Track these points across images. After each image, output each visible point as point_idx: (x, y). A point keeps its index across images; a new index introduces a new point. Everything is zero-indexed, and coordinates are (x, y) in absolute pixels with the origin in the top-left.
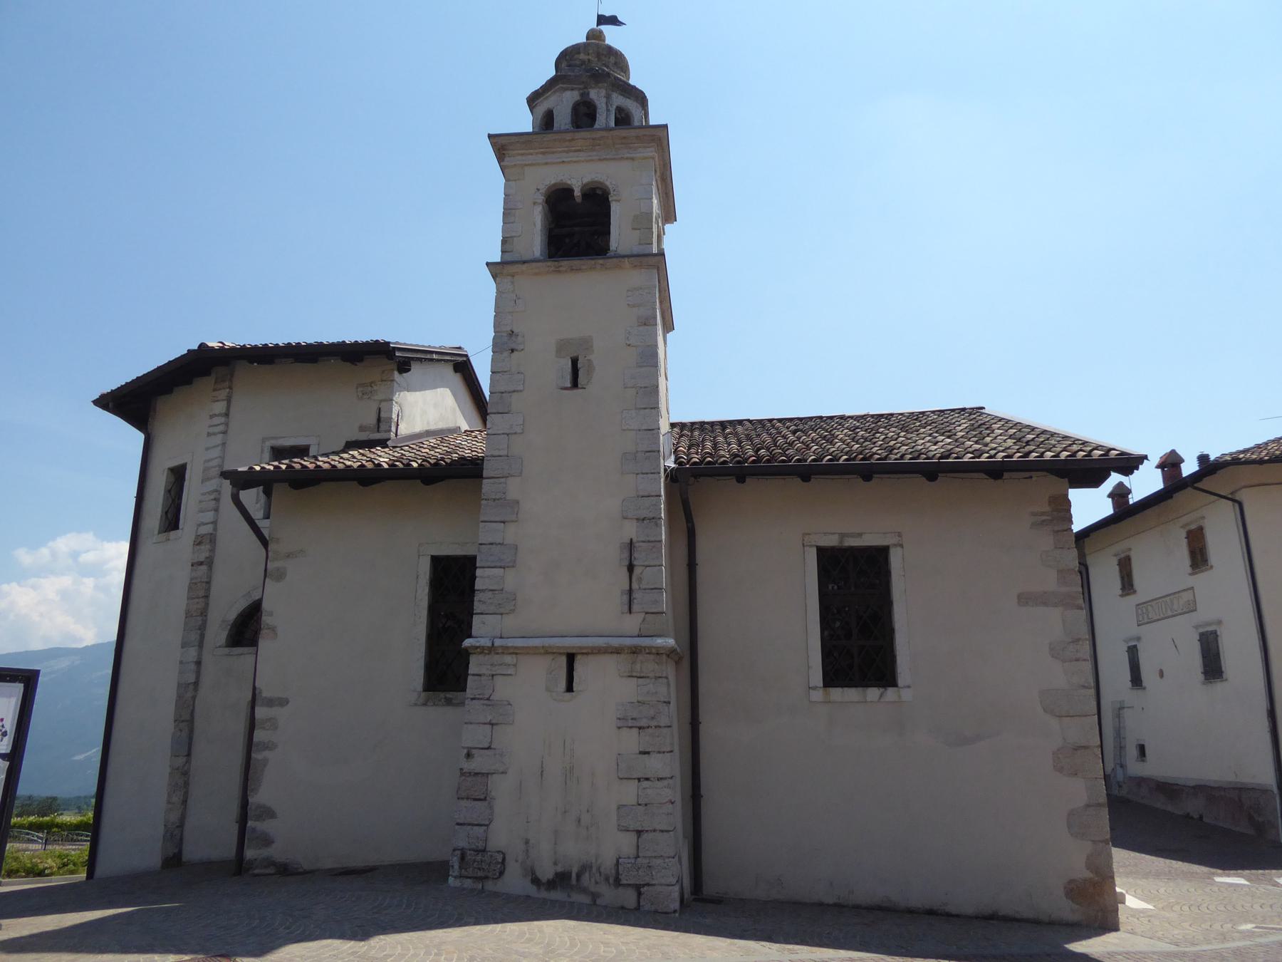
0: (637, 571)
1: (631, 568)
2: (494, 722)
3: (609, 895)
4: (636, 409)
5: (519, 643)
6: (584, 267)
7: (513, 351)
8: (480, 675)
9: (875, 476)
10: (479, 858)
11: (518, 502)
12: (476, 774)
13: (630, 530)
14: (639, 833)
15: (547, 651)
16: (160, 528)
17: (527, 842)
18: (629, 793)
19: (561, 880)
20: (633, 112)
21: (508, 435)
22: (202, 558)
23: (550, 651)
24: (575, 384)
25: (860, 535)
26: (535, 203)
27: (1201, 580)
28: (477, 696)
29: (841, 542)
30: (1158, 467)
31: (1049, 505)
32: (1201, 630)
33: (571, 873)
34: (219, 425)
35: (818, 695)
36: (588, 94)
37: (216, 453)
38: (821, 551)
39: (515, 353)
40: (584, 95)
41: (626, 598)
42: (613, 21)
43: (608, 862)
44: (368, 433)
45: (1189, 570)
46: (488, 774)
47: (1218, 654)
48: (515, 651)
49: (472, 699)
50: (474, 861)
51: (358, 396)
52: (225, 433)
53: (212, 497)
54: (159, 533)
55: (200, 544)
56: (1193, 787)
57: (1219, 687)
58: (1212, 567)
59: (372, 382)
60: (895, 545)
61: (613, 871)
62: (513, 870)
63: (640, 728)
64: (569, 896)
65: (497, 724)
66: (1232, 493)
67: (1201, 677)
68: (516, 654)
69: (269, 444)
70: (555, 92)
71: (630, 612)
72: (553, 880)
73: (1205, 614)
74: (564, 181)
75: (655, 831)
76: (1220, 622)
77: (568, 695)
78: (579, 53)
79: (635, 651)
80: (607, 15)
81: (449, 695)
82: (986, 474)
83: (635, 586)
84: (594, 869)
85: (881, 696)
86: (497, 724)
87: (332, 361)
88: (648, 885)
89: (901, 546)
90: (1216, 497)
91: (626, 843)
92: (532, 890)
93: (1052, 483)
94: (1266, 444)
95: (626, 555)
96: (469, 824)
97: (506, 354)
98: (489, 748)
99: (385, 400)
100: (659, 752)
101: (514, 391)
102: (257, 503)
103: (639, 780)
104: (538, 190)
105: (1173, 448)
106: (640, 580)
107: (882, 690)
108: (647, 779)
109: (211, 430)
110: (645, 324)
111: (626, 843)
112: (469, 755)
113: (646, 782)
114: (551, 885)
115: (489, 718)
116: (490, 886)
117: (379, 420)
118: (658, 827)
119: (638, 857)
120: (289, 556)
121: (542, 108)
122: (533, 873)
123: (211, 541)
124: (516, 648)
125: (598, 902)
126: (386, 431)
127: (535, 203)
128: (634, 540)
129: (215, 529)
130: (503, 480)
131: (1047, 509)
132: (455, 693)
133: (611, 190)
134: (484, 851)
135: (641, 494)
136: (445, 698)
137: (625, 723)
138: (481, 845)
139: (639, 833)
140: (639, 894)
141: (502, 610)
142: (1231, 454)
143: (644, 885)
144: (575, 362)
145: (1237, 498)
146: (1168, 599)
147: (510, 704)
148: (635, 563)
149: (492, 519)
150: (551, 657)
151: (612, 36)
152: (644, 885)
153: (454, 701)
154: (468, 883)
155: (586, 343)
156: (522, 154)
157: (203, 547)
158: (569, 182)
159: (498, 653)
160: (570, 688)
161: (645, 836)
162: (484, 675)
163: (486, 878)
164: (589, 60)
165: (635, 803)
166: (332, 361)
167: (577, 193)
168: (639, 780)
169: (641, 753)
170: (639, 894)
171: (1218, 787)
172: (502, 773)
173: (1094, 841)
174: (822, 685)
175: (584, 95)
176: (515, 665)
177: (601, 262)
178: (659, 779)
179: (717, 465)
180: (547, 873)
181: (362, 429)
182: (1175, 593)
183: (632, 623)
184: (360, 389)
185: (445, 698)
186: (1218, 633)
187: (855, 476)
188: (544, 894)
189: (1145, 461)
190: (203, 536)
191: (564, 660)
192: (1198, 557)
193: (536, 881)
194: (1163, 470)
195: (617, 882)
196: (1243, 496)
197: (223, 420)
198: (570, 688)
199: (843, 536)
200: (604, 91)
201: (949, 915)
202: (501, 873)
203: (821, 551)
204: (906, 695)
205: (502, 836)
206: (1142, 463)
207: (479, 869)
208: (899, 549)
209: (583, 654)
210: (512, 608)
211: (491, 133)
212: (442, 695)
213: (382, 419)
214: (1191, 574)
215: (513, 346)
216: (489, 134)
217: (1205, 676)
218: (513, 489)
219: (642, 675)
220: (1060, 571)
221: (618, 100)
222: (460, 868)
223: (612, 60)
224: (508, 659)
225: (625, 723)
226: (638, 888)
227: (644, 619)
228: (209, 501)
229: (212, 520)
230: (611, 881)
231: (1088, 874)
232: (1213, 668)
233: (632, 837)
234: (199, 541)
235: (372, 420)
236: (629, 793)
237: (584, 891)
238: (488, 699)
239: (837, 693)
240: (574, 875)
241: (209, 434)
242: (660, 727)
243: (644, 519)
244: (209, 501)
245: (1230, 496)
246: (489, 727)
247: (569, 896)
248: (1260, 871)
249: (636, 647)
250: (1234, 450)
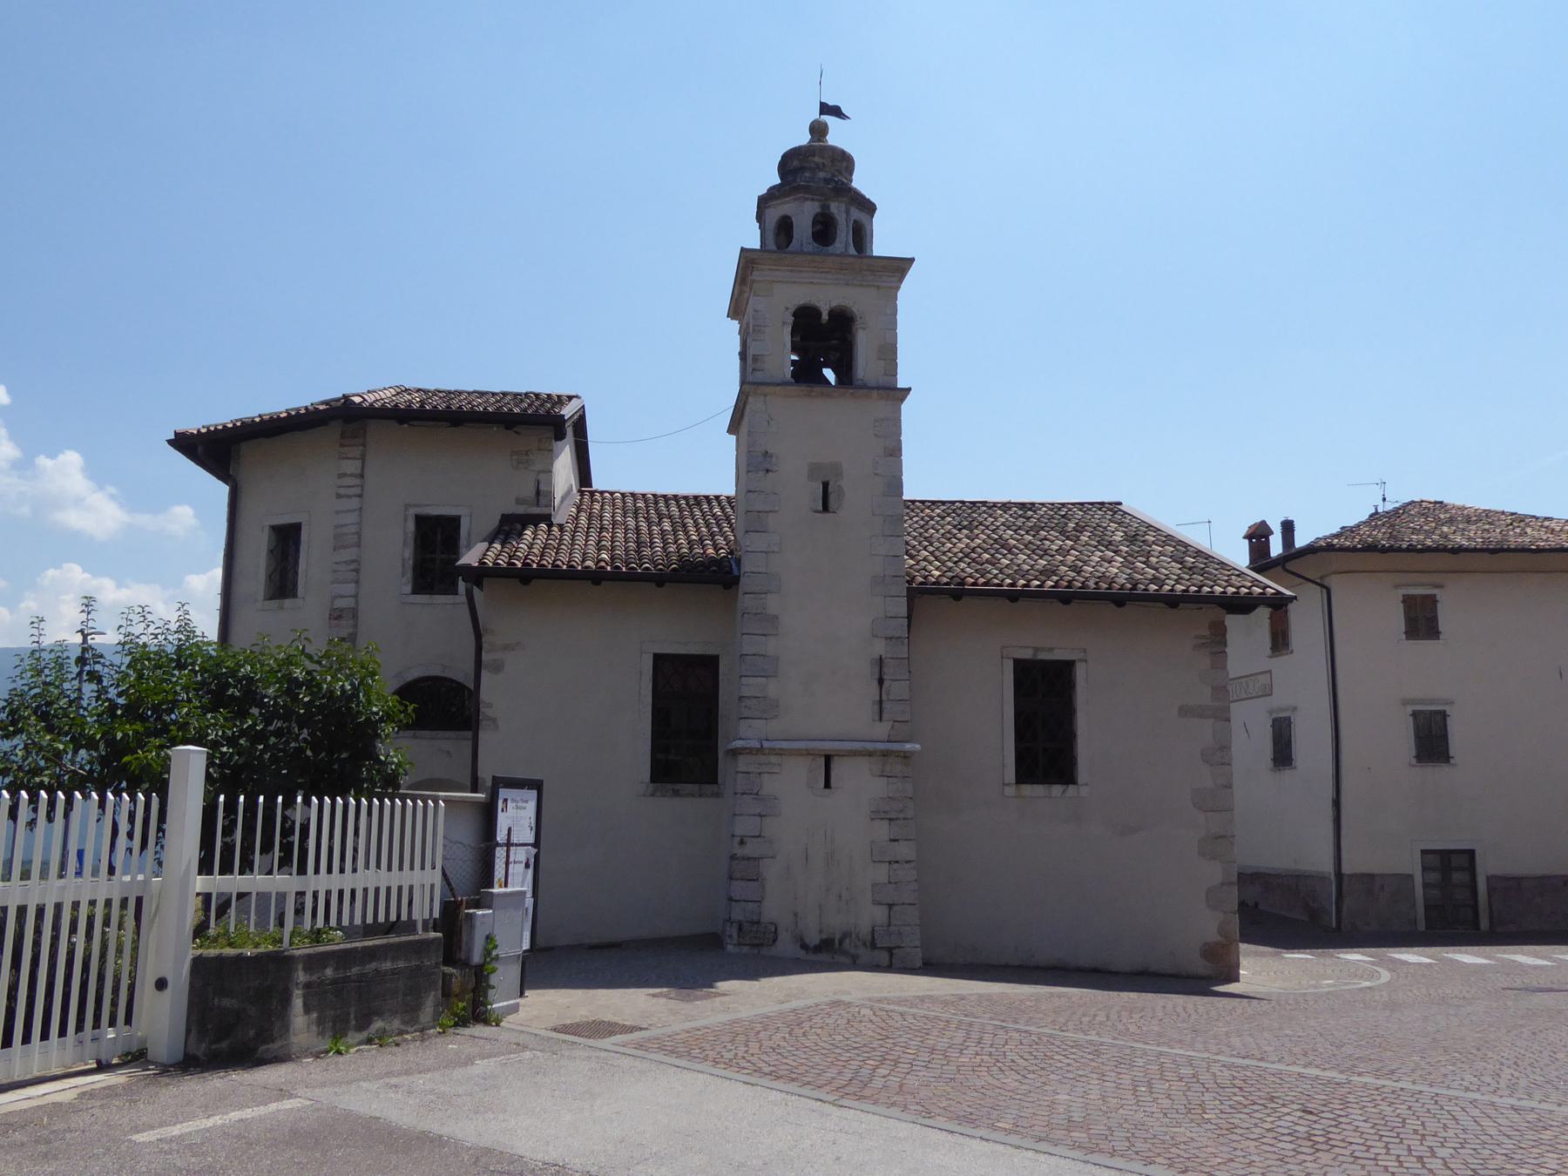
0: (886, 684)
1: (881, 681)
2: (763, 813)
3: (865, 954)
4: (883, 536)
5: (784, 745)
6: (835, 394)
7: (768, 471)
8: (749, 773)
9: (1075, 601)
10: (755, 928)
11: (777, 617)
12: (749, 859)
13: (879, 648)
14: (890, 906)
15: (808, 753)
16: (265, 596)
17: (796, 915)
18: (881, 873)
19: (826, 945)
20: (864, 221)
21: (766, 553)
22: (344, 633)
23: (812, 752)
24: (825, 508)
25: (1051, 650)
26: (784, 323)
27: (1280, 664)
28: (747, 792)
29: (1035, 655)
30: (1244, 538)
31: (1210, 629)
32: (1275, 716)
33: (834, 940)
34: (352, 486)
35: (1010, 791)
36: (828, 207)
37: (352, 518)
38: (1018, 663)
39: (770, 473)
40: (825, 207)
41: (876, 708)
42: (836, 111)
43: (865, 930)
44: (525, 506)
45: (1269, 652)
46: (759, 858)
47: (1290, 741)
48: (781, 753)
49: (743, 794)
50: (751, 931)
51: (512, 465)
52: (360, 496)
53: (352, 567)
54: (264, 600)
55: (339, 617)
56: (1251, 875)
57: (1287, 774)
58: (1292, 652)
59: (527, 451)
60: (1081, 660)
61: (870, 937)
62: (785, 937)
63: (890, 820)
64: (833, 958)
65: (765, 816)
66: (1321, 578)
67: (1271, 764)
68: (781, 754)
69: (413, 511)
70: (795, 200)
71: (881, 720)
72: (819, 945)
73: (1280, 699)
74: (812, 302)
75: (903, 904)
76: (1295, 709)
77: (827, 791)
78: (814, 156)
79: (886, 754)
80: (830, 104)
81: (678, 786)
82: (1167, 604)
83: (884, 697)
84: (854, 936)
85: (1064, 792)
86: (765, 816)
87: (495, 429)
88: (899, 947)
89: (1086, 661)
90: (1301, 580)
91: (880, 914)
92: (801, 954)
93: (1214, 612)
94: (1358, 526)
95: (877, 670)
96: (745, 901)
97: (761, 474)
98: (759, 836)
99: (544, 472)
100: (906, 840)
101: (771, 511)
102: (403, 576)
103: (890, 863)
104: (787, 309)
105: (1263, 519)
106: (888, 694)
107: (1065, 786)
108: (897, 862)
109: (342, 491)
110: (891, 455)
111: (880, 914)
112: (742, 842)
113: (897, 864)
114: (818, 949)
115: (758, 811)
116: (764, 951)
117: (538, 493)
118: (907, 902)
119: (889, 925)
120: (506, 648)
121: (774, 214)
122: (802, 939)
123: (354, 617)
124: (780, 749)
125: (857, 962)
126: (546, 506)
127: (784, 323)
128: (883, 657)
129: (357, 603)
130: (763, 596)
131: (1207, 633)
132: (683, 785)
133: (858, 319)
134: (758, 923)
135: (889, 615)
136: (673, 790)
137: (877, 815)
138: (755, 918)
139: (890, 906)
140: (891, 955)
141: (766, 716)
142: (1325, 538)
143: (895, 948)
144: (826, 485)
145: (1326, 584)
146: (1243, 680)
147: (776, 799)
148: (885, 677)
149: (750, 632)
150: (811, 757)
151: (838, 134)
152: (895, 948)
153: (681, 792)
154: (745, 949)
155: (837, 469)
156: (770, 270)
157: (343, 622)
158: (818, 305)
159: (765, 754)
160: (827, 785)
161: (896, 908)
162: (752, 773)
163: (762, 945)
164: (823, 164)
165: (887, 881)
166: (495, 429)
167: (825, 317)
168: (890, 863)
169: (892, 840)
170: (891, 955)
171: (1276, 875)
172: (772, 857)
173: (1225, 913)
174: (1014, 781)
175: (825, 207)
176: (779, 765)
177: (851, 391)
178: (907, 862)
179: (953, 586)
180: (814, 939)
181: (519, 501)
182: (1251, 675)
183: (882, 729)
184: (515, 457)
185: (673, 790)
186: (1292, 720)
187: (1055, 600)
188: (812, 957)
189: (1295, 601)
190: (342, 610)
191: (823, 759)
192: (1280, 641)
193: (804, 946)
194: (1250, 541)
195: (873, 946)
196: (1334, 582)
197: (358, 481)
198: (827, 785)
199: (1036, 650)
200: (844, 206)
201: (1109, 972)
202: (775, 941)
203: (1018, 663)
204: (1084, 791)
205: (774, 909)
206: (1292, 602)
207: (755, 937)
208: (1084, 664)
209: (839, 755)
210: (776, 714)
211: (746, 247)
212: (669, 786)
213: (541, 493)
214: (1270, 657)
215: (768, 467)
216: (742, 248)
217: (1275, 763)
218: (773, 604)
219: (892, 774)
220: (1213, 688)
221: (856, 214)
222: (739, 936)
223: (845, 164)
224: (773, 759)
225: (877, 815)
226: (890, 950)
227: (892, 727)
228: (347, 571)
229: (353, 593)
230: (868, 944)
231: (1218, 938)
232: (1283, 755)
233: (885, 909)
234: (337, 615)
235: (529, 492)
236: (881, 873)
237: (845, 953)
238: (757, 794)
239: (1028, 790)
240: (837, 942)
241: (339, 496)
242: (907, 819)
243: (891, 638)
244: (347, 571)
245: (1318, 581)
246: (758, 819)
247: (833, 958)
248: (1320, 950)
249: (887, 751)
250: (1328, 534)
